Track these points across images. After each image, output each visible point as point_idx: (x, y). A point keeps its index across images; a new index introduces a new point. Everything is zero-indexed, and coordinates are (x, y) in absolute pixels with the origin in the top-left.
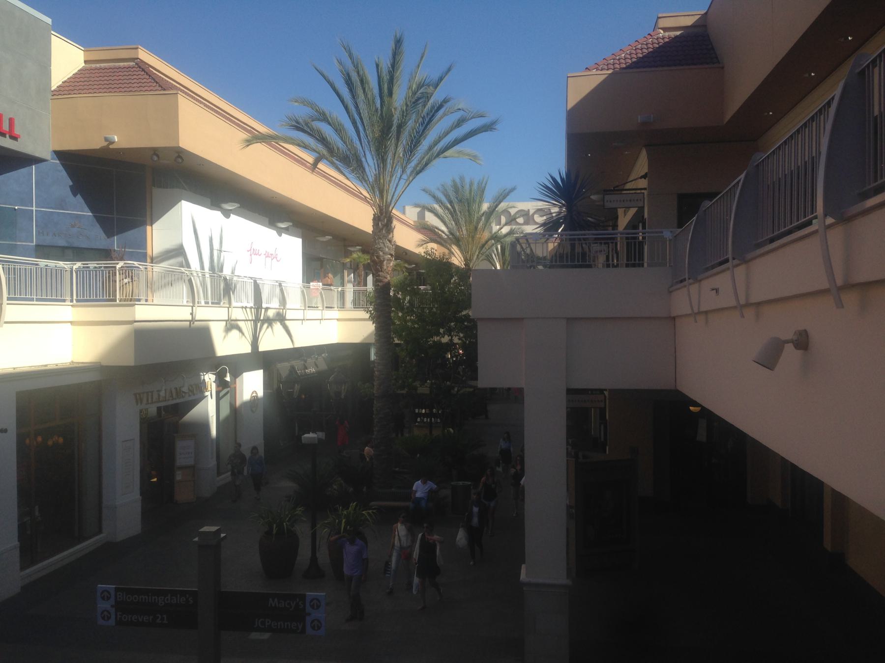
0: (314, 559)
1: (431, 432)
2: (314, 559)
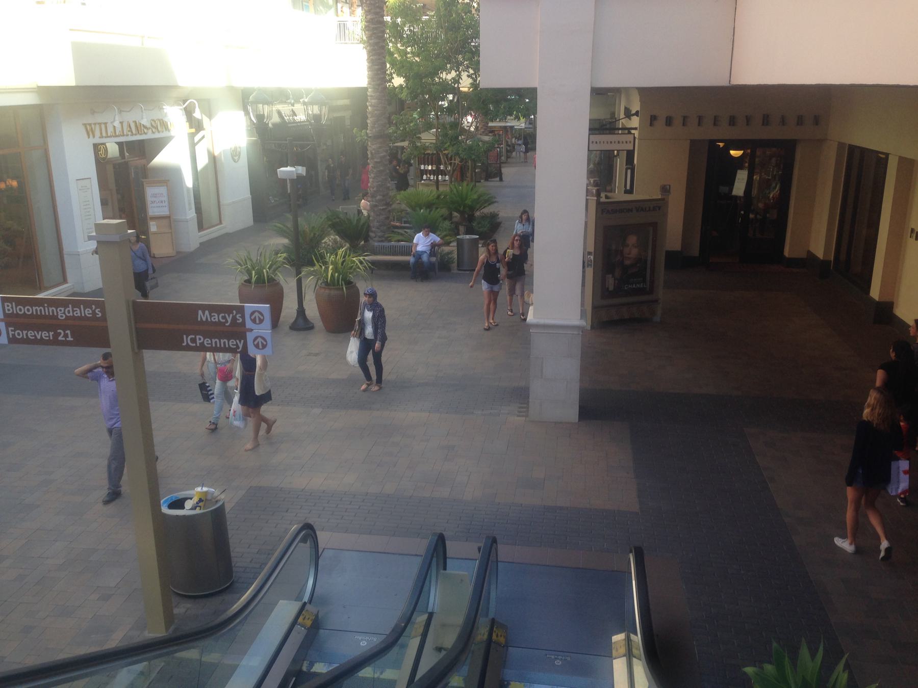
0: (301, 311)
1: (438, 189)
2: (301, 311)
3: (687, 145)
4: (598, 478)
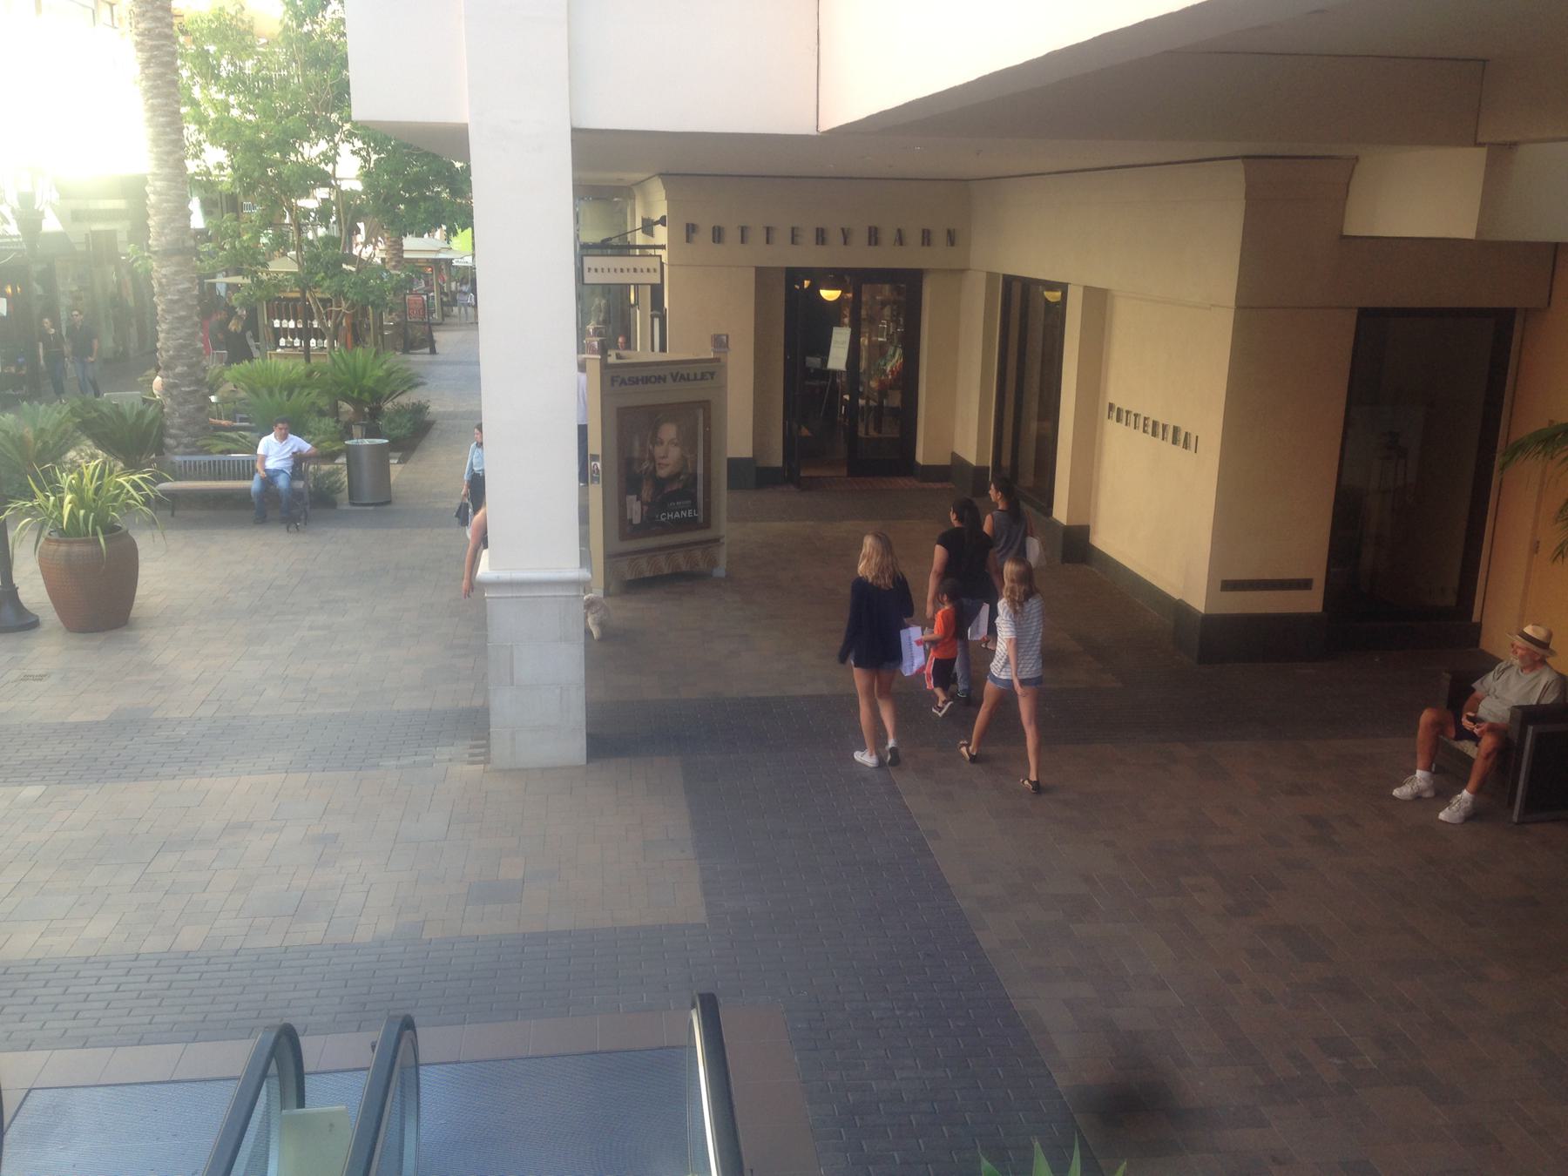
3: (751, 274)
4: (637, 865)
